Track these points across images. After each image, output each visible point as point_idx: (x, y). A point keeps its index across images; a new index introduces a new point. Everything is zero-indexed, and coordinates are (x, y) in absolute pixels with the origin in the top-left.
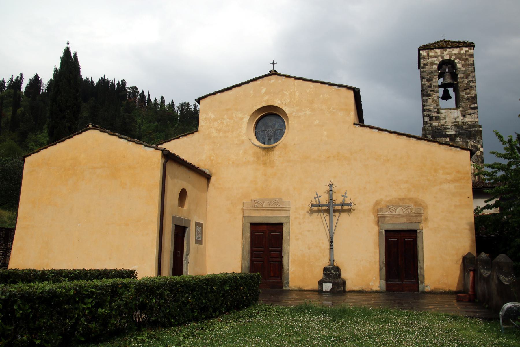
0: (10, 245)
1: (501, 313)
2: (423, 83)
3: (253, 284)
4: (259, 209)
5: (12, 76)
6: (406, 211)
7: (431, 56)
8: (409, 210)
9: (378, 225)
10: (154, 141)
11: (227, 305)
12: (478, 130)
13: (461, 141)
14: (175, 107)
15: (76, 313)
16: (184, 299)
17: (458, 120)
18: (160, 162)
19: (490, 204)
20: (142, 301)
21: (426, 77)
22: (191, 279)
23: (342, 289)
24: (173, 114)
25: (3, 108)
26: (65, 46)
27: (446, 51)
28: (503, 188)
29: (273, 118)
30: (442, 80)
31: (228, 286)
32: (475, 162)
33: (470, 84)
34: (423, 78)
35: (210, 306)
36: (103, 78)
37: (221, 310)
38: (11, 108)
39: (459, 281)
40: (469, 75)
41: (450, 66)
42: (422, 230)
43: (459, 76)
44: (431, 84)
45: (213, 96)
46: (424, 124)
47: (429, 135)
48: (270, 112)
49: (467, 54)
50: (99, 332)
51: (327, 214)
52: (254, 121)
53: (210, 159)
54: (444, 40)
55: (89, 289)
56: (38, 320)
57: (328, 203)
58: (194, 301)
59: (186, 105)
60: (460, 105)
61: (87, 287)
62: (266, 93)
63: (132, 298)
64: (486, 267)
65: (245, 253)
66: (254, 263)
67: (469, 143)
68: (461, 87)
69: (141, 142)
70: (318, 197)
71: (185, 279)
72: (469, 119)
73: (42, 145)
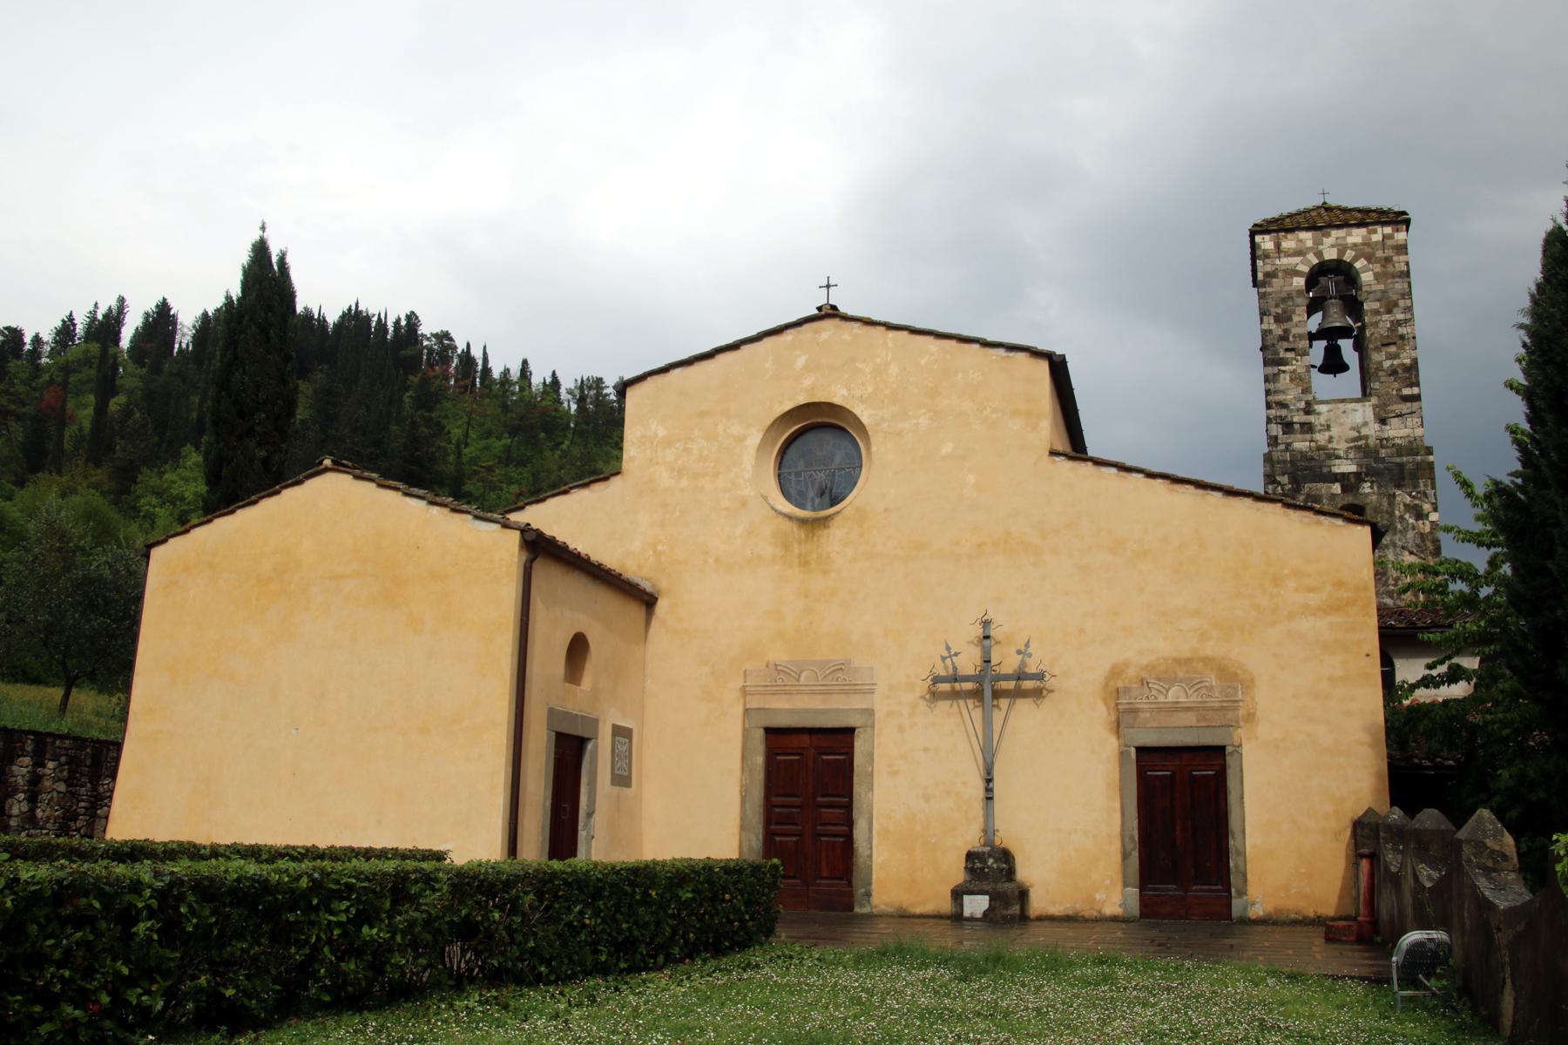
0: (105, 787)
1: (1394, 959)
3: (758, 888)
4: (787, 688)
5: (96, 304)
6: (1196, 694)
7: (1285, 252)
8: (1204, 691)
9: (1118, 733)
10: (502, 490)
11: (686, 941)
12: (1423, 461)
13: (1373, 493)
14: (563, 391)
15: (312, 935)
16: (571, 918)
17: (1364, 431)
18: (516, 560)
19: (1435, 675)
20: (468, 916)
21: (1273, 310)
22: (591, 866)
23: (1018, 912)
24: (556, 410)
25: (69, 395)
26: (255, 236)
27: (1328, 235)
28: (1475, 628)
29: (828, 438)
30: (1317, 318)
31: (690, 889)
32: (1415, 551)
33: (1400, 329)
35: (641, 938)
36: (353, 308)
37: (672, 951)
38: (92, 397)
39: (1344, 889)
40: (1396, 304)
41: (1341, 278)
42: (1240, 745)
44: (1286, 331)
45: (662, 375)
48: (819, 420)
49: (1389, 246)
50: (363, 983)
51: (976, 704)
52: (775, 444)
53: (655, 552)
54: (1325, 203)
55: (342, 879)
56: (230, 944)
57: (978, 673)
58: (599, 924)
59: (594, 385)
60: (1371, 389)
61: (336, 873)
63: (443, 906)
64: (1401, 847)
65: (749, 812)
67: (1398, 499)
68: (1373, 337)
69: (465, 507)
70: (950, 656)
71: (575, 866)
72: (1397, 431)
73: (178, 503)
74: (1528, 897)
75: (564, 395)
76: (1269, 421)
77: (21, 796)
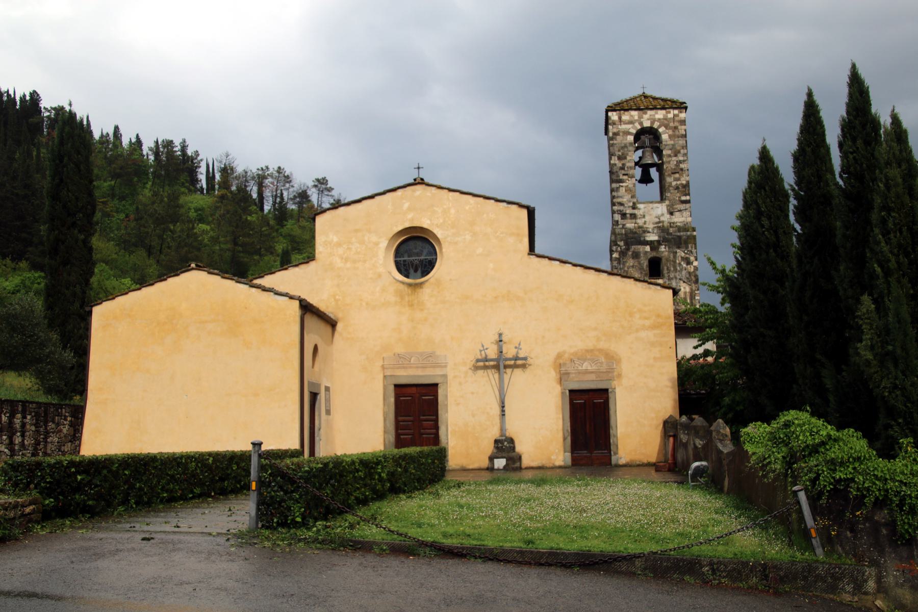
2: (612, 162)
8: (599, 364)
9: (561, 384)
12: (691, 235)
17: (662, 219)
21: (617, 153)
27: (646, 113)
29: (419, 244)
33: (681, 165)
34: (613, 155)
39: (659, 450)
40: (679, 152)
41: (651, 136)
42: (615, 388)
43: (664, 152)
44: (623, 165)
45: (334, 210)
46: (613, 225)
47: (621, 241)
54: (644, 93)
62: (410, 209)
65: (388, 425)
66: (401, 438)
67: (678, 254)
70: (484, 350)
74: (733, 448)
75: (145, 150)
76: (613, 212)
77: (19, 434)
